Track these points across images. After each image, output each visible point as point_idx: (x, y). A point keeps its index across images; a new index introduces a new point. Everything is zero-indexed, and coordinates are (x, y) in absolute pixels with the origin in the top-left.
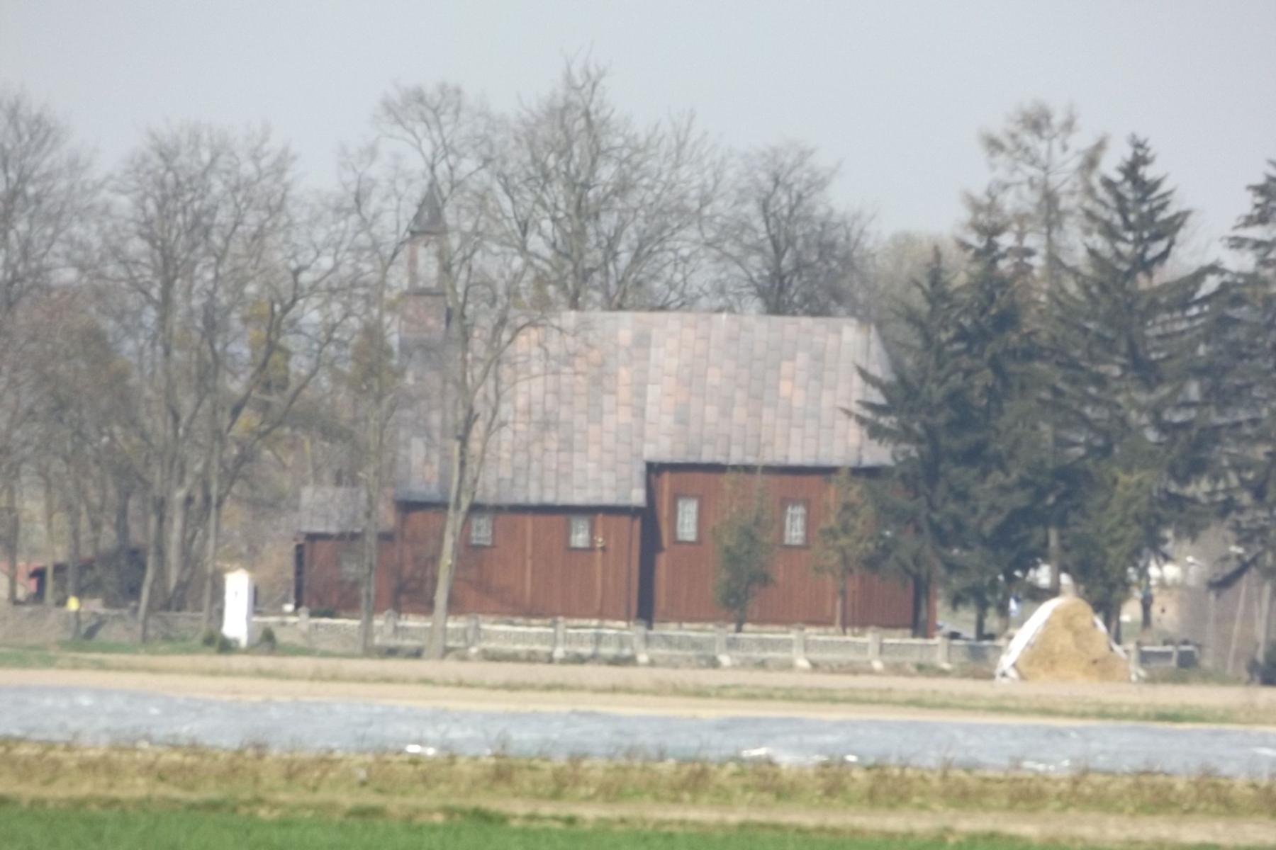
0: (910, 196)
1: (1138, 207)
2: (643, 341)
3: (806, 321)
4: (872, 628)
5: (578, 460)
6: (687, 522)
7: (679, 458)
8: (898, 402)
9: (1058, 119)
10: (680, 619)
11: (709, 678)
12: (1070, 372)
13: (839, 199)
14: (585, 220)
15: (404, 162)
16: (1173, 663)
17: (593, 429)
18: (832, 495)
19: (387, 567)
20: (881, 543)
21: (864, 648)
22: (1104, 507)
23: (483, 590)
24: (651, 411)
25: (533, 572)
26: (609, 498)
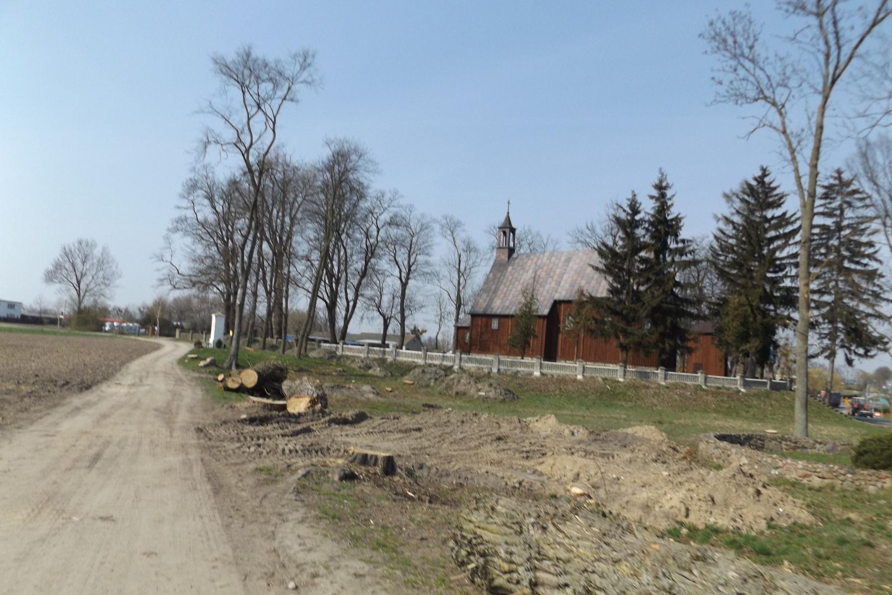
11: (606, 376)
20: (499, 274)
24: (562, 283)
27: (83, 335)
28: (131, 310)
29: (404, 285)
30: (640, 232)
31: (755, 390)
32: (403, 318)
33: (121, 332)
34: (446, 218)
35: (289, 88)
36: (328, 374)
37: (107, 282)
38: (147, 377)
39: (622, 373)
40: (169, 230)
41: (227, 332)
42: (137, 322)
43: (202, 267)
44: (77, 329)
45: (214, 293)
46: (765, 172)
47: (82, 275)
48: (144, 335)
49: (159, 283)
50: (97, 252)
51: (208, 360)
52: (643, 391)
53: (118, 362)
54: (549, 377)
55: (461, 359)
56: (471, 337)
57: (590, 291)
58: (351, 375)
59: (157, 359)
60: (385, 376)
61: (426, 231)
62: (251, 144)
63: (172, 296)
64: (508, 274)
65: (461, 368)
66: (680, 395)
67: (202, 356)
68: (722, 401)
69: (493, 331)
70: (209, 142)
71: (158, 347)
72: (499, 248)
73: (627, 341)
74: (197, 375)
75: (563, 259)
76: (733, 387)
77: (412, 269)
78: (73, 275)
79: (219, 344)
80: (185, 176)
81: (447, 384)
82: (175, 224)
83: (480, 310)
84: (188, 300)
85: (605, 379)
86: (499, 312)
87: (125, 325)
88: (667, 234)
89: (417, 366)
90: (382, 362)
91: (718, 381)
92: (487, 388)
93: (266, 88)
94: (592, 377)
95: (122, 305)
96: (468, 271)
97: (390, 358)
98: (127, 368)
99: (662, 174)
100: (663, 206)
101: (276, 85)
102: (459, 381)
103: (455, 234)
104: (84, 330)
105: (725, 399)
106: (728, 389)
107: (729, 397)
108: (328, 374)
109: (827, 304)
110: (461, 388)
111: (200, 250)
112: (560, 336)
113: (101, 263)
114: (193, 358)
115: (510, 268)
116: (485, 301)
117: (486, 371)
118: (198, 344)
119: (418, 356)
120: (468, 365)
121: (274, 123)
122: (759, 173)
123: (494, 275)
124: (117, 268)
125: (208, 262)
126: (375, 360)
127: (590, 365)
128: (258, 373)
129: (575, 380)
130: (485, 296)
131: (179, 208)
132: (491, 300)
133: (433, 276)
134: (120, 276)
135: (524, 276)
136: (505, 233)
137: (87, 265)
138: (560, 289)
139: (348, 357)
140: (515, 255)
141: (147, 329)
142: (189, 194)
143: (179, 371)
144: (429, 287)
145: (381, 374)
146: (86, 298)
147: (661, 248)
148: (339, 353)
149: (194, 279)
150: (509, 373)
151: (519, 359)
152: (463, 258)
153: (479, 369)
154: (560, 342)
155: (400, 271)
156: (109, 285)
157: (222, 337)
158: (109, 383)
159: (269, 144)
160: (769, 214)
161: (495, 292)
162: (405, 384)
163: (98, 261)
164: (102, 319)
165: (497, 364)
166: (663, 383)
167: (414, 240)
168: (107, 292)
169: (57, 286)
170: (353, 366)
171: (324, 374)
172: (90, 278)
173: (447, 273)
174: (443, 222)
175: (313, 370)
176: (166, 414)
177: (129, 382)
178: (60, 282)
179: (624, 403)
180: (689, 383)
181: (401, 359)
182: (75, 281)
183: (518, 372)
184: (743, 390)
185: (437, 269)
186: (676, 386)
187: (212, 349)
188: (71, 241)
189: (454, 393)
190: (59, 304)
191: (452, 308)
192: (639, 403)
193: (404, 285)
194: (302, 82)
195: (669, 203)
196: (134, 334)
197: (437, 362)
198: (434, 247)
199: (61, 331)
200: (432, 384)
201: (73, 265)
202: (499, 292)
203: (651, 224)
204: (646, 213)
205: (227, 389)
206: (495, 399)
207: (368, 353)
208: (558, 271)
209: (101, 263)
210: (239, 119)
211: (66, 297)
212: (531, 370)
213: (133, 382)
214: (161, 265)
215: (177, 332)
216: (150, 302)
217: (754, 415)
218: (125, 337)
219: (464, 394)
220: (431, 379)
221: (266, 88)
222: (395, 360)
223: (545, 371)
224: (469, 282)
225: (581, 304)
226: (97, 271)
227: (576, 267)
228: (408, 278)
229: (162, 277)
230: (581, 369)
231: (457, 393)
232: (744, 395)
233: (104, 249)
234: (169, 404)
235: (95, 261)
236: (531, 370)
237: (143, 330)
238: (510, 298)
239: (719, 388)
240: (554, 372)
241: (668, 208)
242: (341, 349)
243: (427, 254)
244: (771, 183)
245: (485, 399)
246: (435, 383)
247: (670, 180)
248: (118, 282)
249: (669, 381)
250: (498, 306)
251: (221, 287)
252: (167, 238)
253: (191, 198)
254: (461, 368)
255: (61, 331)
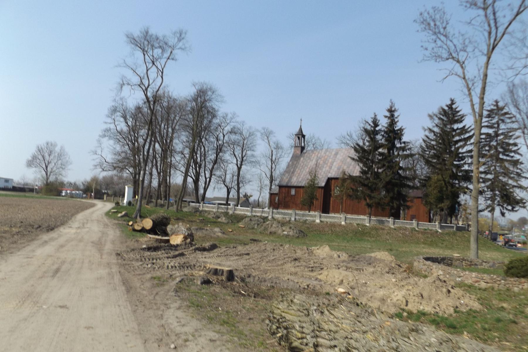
11: (359, 222)
20: (295, 162)
24: (333, 167)
27: (49, 198)
28: (77, 183)
29: (239, 169)
30: (379, 137)
31: (447, 230)
32: (239, 188)
33: (72, 196)
34: (264, 129)
35: (171, 52)
36: (194, 221)
37: (63, 167)
38: (87, 223)
39: (368, 221)
40: (100, 136)
41: (134, 197)
42: (81, 190)
43: (120, 158)
44: (45, 195)
45: (127, 174)
46: (453, 102)
47: (49, 163)
48: (85, 198)
49: (94, 167)
50: (58, 149)
51: (123, 213)
52: (381, 231)
53: (70, 214)
54: (325, 223)
55: (273, 212)
56: (279, 199)
57: (349, 172)
58: (208, 222)
59: (93, 213)
60: (228, 223)
61: (252, 137)
62: (149, 85)
63: (102, 175)
64: (300, 162)
65: (273, 218)
66: (402, 234)
67: (120, 211)
68: (428, 237)
69: (292, 196)
70: (124, 84)
71: (93, 205)
72: (296, 147)
73: (371, 202)
74: (117, 222)
75: (333, 153)
76: (434, 229)
77: (244, 159)
78: (43, 162)
79: (129, 203)
80: (109, 104)
81: (265, 227)
82: (104, 133)
83: (284, 183)
84: (112, 178)
85: (358, 224)
86: (295, 185)
87: (74, 192)
88: (395, 138)
89: (247, 217)
90: (226, 214)
91: (425, 225)
92: (288, 229)
93: (157, 52)
94: (350, 223)
95: (72, 181)
96: (277, 161)
97: (231, 212)
98: (75, 217)
99: (392, 103)
100: (392, 122)
101: (163, 50)
102: (272, 226)
103: (269, 139)
104: (50, 195)
105: (429, 236)
106: (431, 230)
107: (431, 235)
108: (194, 221)
109: (489, 180)
110: (273, 230)
111: (118, 148)
112: (332, 199)
113: (60, 156)
114: (114, 212)
115: (302, 159)
116: (287, 178)
117: (288, 219)
118: (117, 204)
119: (247, 211)
120: (277, 216)
121: (162, 73)
122: (449, 102)
123: (293, 163)
124: (69, 158)
125: (123, 155)
126: (222, 213)
127: (349, 216)
128: (153, 221)
129: (340, 225)
130: (287, 175)
131: (106, 123)
132: (291, 178)
133: (256, 163)
134: (71, 164)
135: (310, 164)
136: (299, 138)
137: (52, 157)
138: (331, 171)
139: (206, 211)
140: (305, 151)
141: (87, 195)
142: (112, 114)
143: (106, 220)
144: (254, 170)
145: (225, 221)
146: (51, 176)
147: (391, 147)
148: (201, 209)
149: (115, 165)
150: (301, 221)
151: (307, 212)
152: (274, 153)
153: (283, 218)
154: (331, 202)
155: (237, 161)
156: (64, 169)
157: (131, 199)
158: (65, 226)
159: (159, 85)
160: (455, 126)
161: (293, 173)
162: (240, 227)
163: (58, 155)
164: (60, 189)
165: (294, 215)
166: (393, 227)
167: (245, 142)
168: (63, 173)
169: (34, 169)
170: (209, 216)
171: (192, 221)
172: (53, 164)
173: (264, 162)
174: (263, 131)
175: (185, 219)
176: (99, 245)
177: (77, 226)
178: (35, 167)
179: (369, 239)
180: (408, 226)
181: (237, 212)
182: (44, 166)
183: (307, 220)
184: (440, 231)
185: (259, 159)
186: (400, 228)
187: (125, 207)
188: (42, 142)
189: (268, 233)
190: (35, 180)
191: (268, 182)
192: (378, 238)
193: (239, 169)
194: (179, 49)
195: (396, 120)
196: (79, 198)
197: (259, 214)
198: (257, 146)
199: (36, 196)
200: (256, 227)
201: (43, 157)
202: (295, 173)
203: (385, 132)
204: (383, 126)
205: (134, 230)
206: (293, 236)
207: (218, 209)
208: (330, 160)
209: (60, 156)
210: (142, 70)
211: (39, 176)
212: (314, 219)
213: (79, 226)
214: (95, 156)
215: (105, 196)
216: (89, 179)
217: (446, 246)
218: (74, 199)
219: (275, 233)
220: (255, 224)
221: (157, 52)
222: (234, 213)
223: (322, 219)
224: (277, 167)
225: (344, 180)
226: (58, 160)
227: (341, 158)
228: (241, 165)
229: (96, 164)
230: (344, 218)
231: (271, 233)
232: (441, 233)
233: (62, 147)
234: (100, 239)
235: (56, 154)
236: (314, 219)
237: (85, 195)
238: (302, 176)
239: (425, 230)
240: (328, 220)
241: (396, 123)
242: (202, 207)
243: (253, 150)
244: (456, 108)
245: (287, 236)
246: (257, 226)
247: (396, 107)
248: (70, 167)
249: (396, 225)
250: (295, 181)
251: (131, 170)
252: (99, 141)
253: (113, 117)
254: (273, 218)
255: (36, 196)
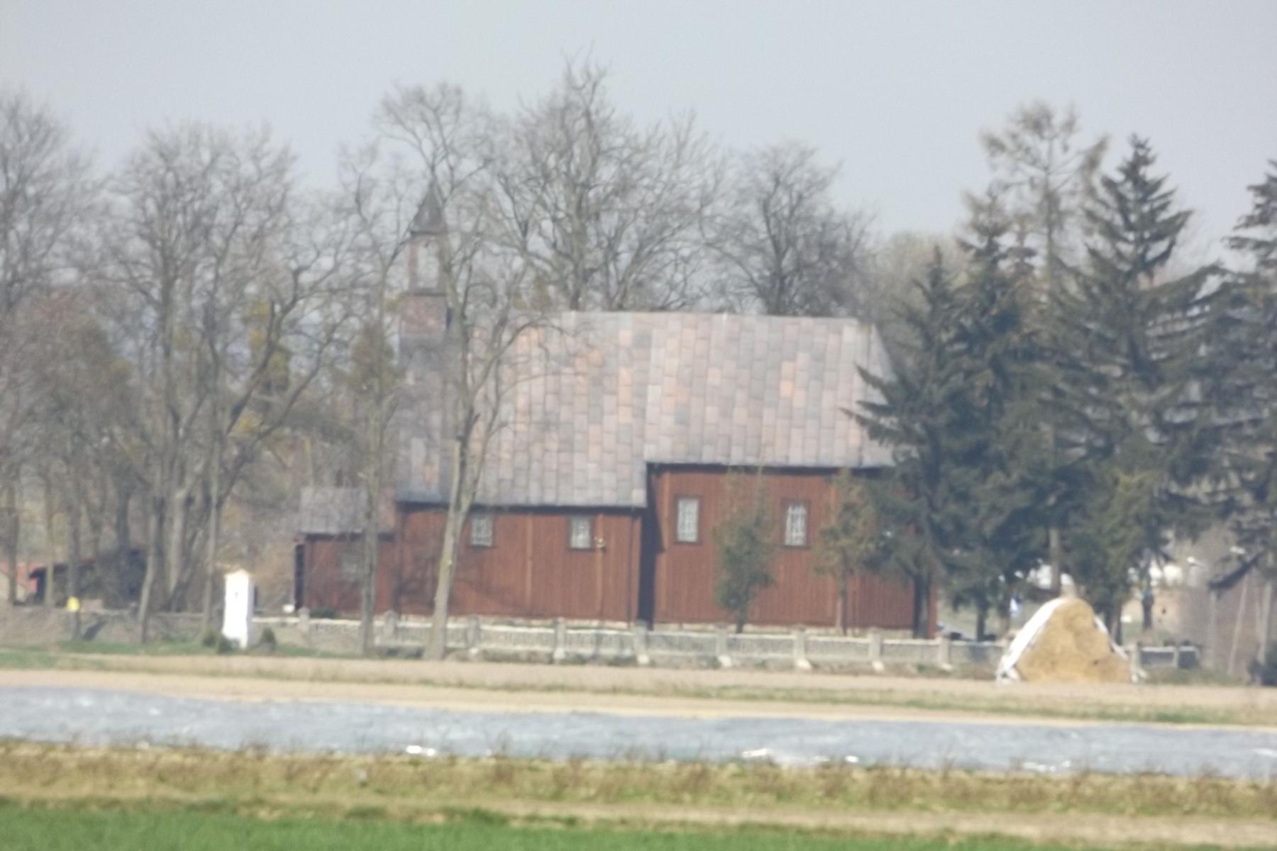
0: (911, 197)
1: (1139, 207)
2: (643, 341)
3: (807, 322)
4: (873, 629)
5: (578, 460)
6: (687, 523)
7: (680, 458)
8: (899, 402)
9: (1059, 119)
10: (681, 620)
11: (709, 678)
12: (1071, 372)
13: (840, 199)
14: (586, 221)
15: (405, 162)
16: (1174, 664)
17: (594, 430)
18: (833, 496)
19: (387, 568)
21: (865, 649)
22: (1104, 508)
23: (484, 591)
24: (651, 412)
25: (534, 573)
26: (609, 499)
134: (294, 158)
230: (878, 648)
